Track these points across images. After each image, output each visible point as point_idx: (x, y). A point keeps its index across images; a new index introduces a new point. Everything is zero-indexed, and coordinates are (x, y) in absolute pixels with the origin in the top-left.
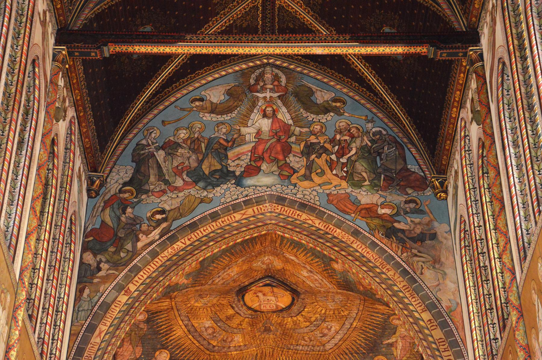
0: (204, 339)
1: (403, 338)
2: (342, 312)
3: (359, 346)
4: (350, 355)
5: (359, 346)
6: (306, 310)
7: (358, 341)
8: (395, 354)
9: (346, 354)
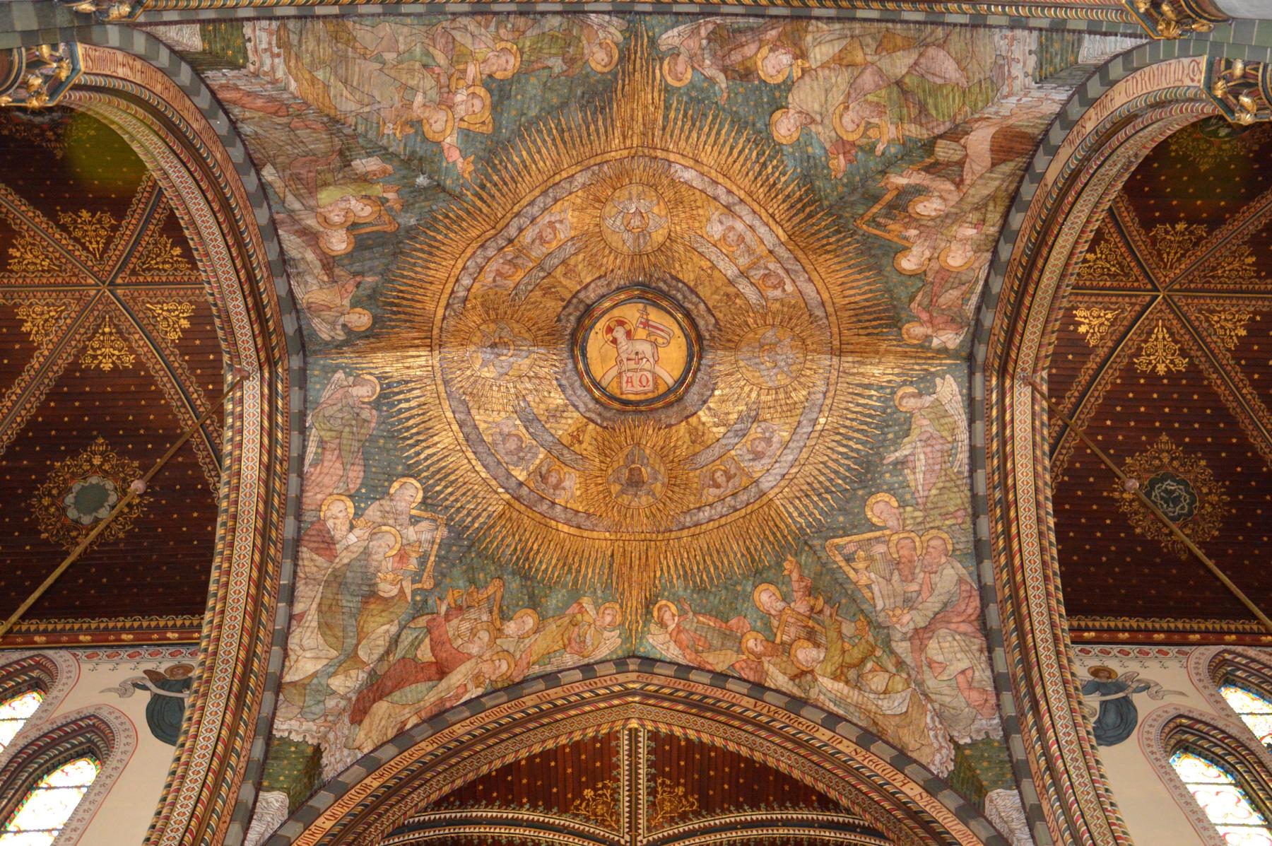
0: (499, 463)
1: (927, 442)
2: (793, 394)
3: (833, 476)
4: (816, 499)
5: (833, 476)
6: (717, 393)
7: (830, 463)
8: (912, 484)
9: (807, 496)
